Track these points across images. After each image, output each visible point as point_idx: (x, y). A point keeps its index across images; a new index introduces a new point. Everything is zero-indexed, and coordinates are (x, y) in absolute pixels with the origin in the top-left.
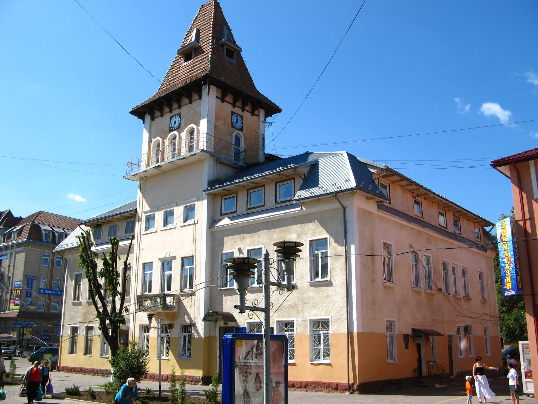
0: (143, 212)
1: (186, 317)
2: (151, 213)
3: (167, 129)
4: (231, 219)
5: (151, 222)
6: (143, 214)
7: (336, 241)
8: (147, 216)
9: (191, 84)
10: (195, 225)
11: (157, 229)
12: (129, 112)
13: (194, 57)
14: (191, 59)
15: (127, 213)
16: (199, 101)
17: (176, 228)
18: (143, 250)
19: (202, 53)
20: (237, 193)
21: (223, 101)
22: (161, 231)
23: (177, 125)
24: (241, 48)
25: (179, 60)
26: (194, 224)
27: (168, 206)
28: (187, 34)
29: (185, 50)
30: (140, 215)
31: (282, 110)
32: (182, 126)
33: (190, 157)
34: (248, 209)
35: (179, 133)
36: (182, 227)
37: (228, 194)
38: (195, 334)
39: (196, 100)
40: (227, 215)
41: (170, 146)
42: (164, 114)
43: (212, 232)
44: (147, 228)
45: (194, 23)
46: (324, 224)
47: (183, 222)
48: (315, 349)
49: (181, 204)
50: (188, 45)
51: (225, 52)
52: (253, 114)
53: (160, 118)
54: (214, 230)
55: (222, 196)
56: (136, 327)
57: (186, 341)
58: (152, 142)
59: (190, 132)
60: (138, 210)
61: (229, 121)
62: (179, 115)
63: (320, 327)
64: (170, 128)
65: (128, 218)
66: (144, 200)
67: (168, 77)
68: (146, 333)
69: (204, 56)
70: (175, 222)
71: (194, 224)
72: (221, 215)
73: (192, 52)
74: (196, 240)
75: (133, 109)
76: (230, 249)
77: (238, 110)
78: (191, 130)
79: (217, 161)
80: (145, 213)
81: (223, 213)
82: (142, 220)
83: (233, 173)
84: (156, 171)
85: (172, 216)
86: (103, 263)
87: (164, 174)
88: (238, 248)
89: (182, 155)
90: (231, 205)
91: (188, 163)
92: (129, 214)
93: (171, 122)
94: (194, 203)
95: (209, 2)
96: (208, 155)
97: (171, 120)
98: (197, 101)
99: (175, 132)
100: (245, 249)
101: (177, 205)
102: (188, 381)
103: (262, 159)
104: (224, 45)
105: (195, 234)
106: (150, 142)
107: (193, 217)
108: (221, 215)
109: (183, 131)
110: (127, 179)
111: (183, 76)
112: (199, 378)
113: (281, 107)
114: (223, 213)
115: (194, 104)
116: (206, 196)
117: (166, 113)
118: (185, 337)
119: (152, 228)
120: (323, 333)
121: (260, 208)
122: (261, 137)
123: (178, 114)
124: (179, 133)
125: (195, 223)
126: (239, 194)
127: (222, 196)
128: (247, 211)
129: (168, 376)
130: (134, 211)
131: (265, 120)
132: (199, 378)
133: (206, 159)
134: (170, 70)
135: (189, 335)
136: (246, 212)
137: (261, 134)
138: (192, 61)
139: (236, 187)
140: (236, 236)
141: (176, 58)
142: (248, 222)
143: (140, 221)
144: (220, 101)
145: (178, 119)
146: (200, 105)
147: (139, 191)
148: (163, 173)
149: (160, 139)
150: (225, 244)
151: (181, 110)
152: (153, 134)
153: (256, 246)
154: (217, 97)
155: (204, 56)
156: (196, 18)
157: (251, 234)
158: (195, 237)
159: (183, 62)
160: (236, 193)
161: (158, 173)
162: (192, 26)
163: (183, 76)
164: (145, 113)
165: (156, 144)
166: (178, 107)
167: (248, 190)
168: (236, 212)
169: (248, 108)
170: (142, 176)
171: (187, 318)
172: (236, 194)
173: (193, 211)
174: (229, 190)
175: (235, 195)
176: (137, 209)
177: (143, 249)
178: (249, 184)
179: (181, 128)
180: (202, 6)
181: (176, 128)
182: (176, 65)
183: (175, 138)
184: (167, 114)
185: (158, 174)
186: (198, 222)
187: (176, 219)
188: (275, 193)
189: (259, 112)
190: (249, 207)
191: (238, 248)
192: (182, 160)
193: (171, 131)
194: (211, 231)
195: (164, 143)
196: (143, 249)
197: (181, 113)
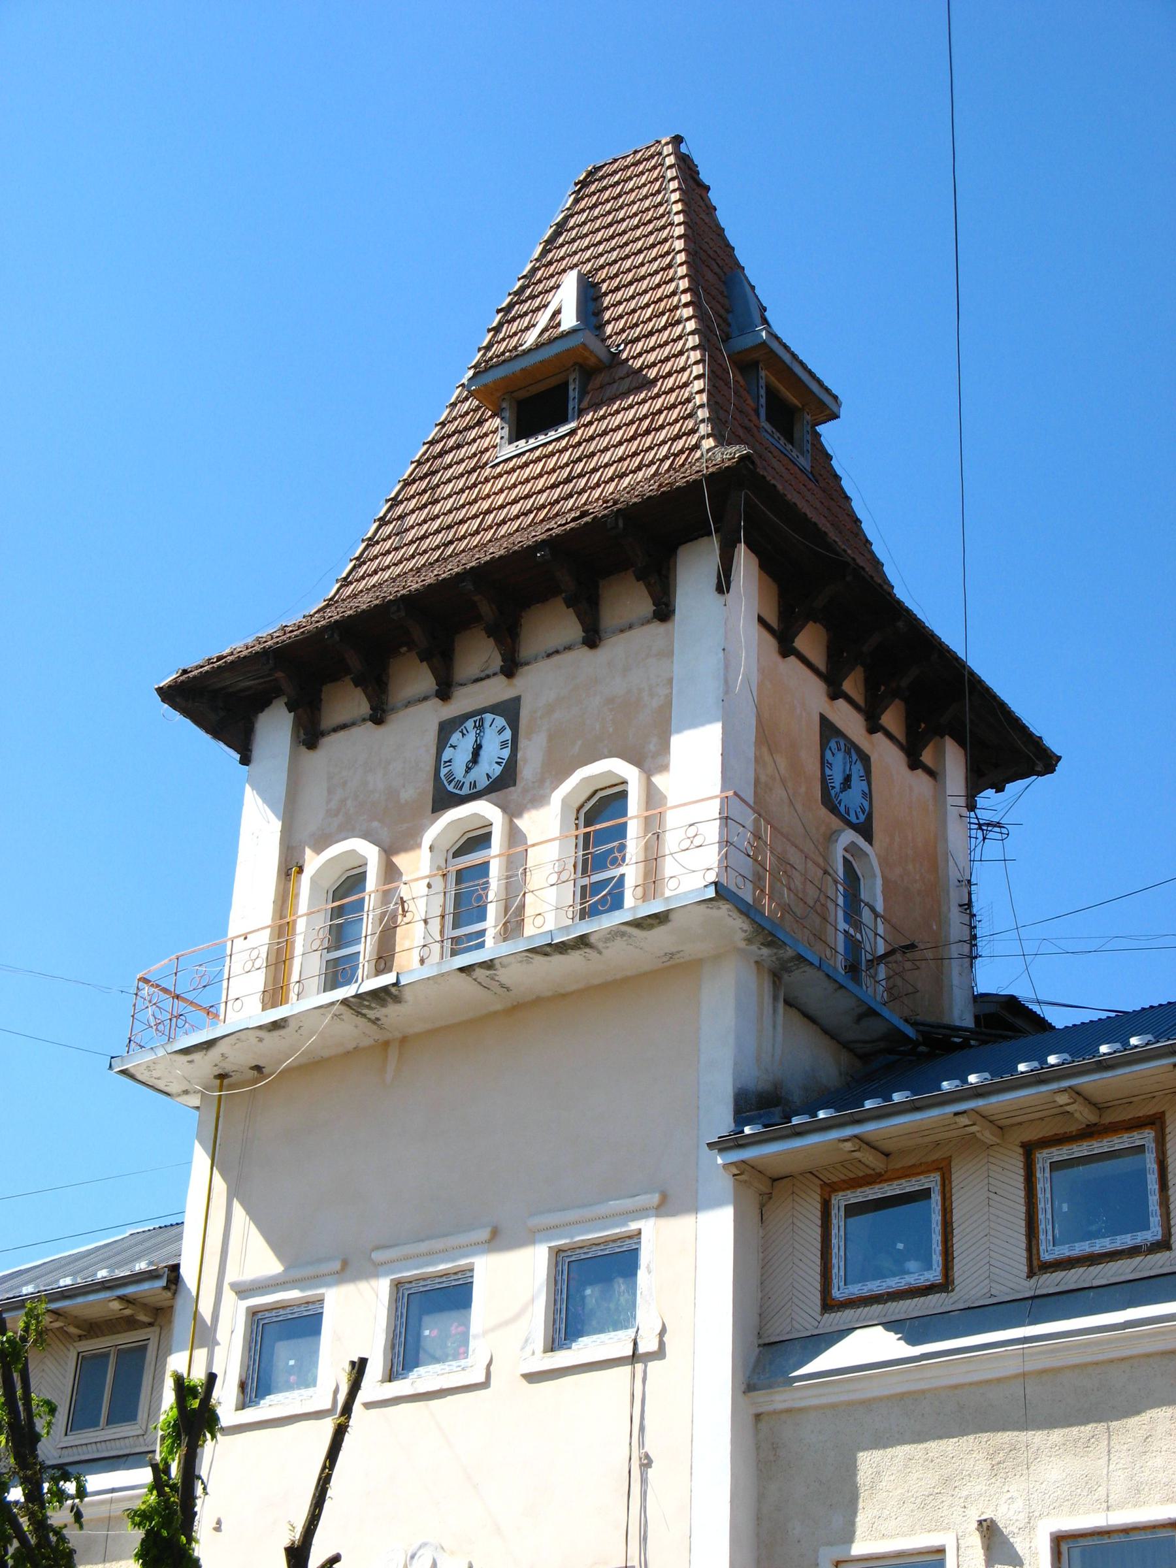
0: (233, 1286)
2: (293, 1294)
3: (420, 788)
4: (911, 1330)
5: (285, 1355)
6: (229, 1296)
8: (254, 1314)
9: (621, 524)
10: (639, 1367)
12: (160, 691)
13: (581, 413)
14: (565, 421)
15: (109, 1288)
16: (657, 628)
17: (485, 1385)
18: (218, 1529)
19: (638, 389)
20: (944, 1169)
21: (786, 649)
23: (489, 766)
24: (835, 398)
25: (473, 434)
26: (635, 1357)
27: (423, 1247)
28: (511, 306)
29: (522, 370)
30: (206, 1309)
31: (1059, 758)
32: (528, 770)
33: (623, 934)
34: (1037, 1267)
35: (512, 812)
36: (533, 1378)
37: (880, 1175)
39: (631, 627)
40: (877, 1309)
41: (439, 884)
42: (394, 710)
43: (758, 1417)
44: (251, 1386)
45: (545, 252)
47: (545, 1351)
49: (529, 1238)
50: (538, 346)
51: (763, 401)
52: (914, 763)
53: (366, 733)
54: (780, 1399)
55: (829, 1189)
58: (301, 870)
59: (582, 806)
60: (188, 1274)
61: (812, 766)
62: (510, 711)
64: (435, 788)
65: (93, 1328)
67: (401, 517)
69: (658, 404)
70: (479, 1351)
71: (635, 1357)
72: (829, 1305)
73: (566, 385)
74: (647, 1463)
75: (185, 672)
76: (912, 1531)
77: (849, 721)
78: (589, 798)
79: (774, 983)
80: (243, 1291)
81: (839, 1292)
82: (222, 1334)
83: (841, 1074)
84: (351, 1030)
85: (462, 1311)
86: (143, 1541)
87: (393, 1053)
88: (980, 1523)
89: (529, 930)
91: (550, 994)
92: (120, 1298)
93: (447, 754)
94: (633, 1226)
95: (636, 152)
96: (737, 925)
97: (443, 741)
99: (484, 809)
100: (1029, 1525)
103: (962, 1015)
104: (755, 365)
105: (642, 1429)
106: (290, 868)
107: (622, 1318)
108: (829, 1305)
109: (538, 800)
110: (132, 1077)
111: (515, 509)
113: (1052, 742)
114: (839, 1292)
115: (614, 649)
116: (724, 1183)
117: (408, 704)
119: (289, 1387)
121: (1139, 1259)
122: (956, 897)
123: (495, 709)
124: (512, 812)
125: (642, 1349)
126: (957, 1177)
127: (829, 1189)
128: (1027, 1283)
130: (162, 1282)
131: (972, 806)
133: (717, 958)
134: (407, 483)
136: (1027, 1288)
137: (954, 874)
138: (573, 432)
139: (964, 1120)
140: (949, 1446)
141: (443, 424)
142: (1053, 1351)
143: (201, 1346)
144: (771, 643)
145: (501, 731)
146: (668, 653)
147: (201, 1159)
148: (386, 1044)
149: (370, 853)
150: (863, 1495)
152: (312, 819)
153: (1121, 1505)
154: (761, 620)
155: (658, 404)
156: (560, 228)
157: (1075, 1430)
158: (641, 1444)
159: (505, 440)
160: (937, 1169)
161: (351, 1047)
162: (534, 270)
163: (515, 509)
164: (261, 702)
165: (333, 880)
166: (497, 662)
167: (1029, 1150)
168: (946, 1285)
169: (891, 719)
170: (237, 1058)
172: (937, 1177)
173: (620, 1285)
174: (887, 1146)
175: (932, 1181)
176: (183, 1271)
177: (219, 1522)
178: (1063, 1099)
179: (520, 784)
180: (590, 174)
181: (483, 783)
182: (448, 459)
183: (479, 840)
184: (412, 710)
185: (352, 1054)
186: (662, 1344)
187: (485, 1333)
189: (940, 754)
190: (1046, 1257)
191: (980, 1523)
192: (557, 959)
193: (444, 799)
194: (754, 1410)
195: (391, 872)
196: (219, 1522)
197: (517, 700)
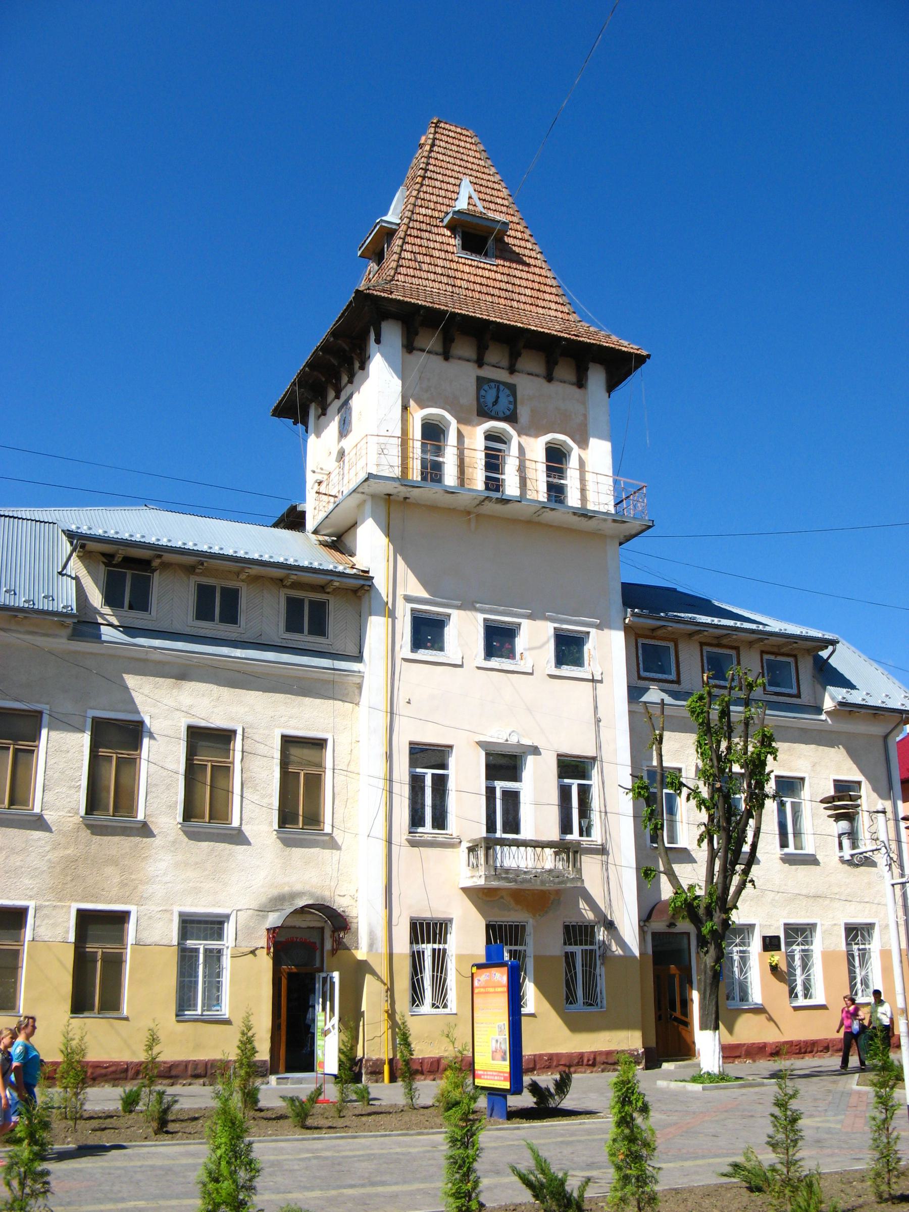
1: (582, 905)
7: (875, 789)
11: (463, 658)
22: (479, 668)
38: (614, 947)
39: (565, 382)
46: (853, 755)
48: (809, 975)
56: (394, 922)
57: (575, 968)
63: (859, 937)
66: (399, 558)
68: (429, 942)
90: (429, 637)
98: (567, 386)
101: (468, 605)
102: (604, 1063)
112: (638, 1054)
118: (569, 958)
120: (859, 950)
129: (537, 1058)
132: (638, 1054)
135: (585, 952)
151: (512, 376)
171: (587, 908)
188: (700, 664)
